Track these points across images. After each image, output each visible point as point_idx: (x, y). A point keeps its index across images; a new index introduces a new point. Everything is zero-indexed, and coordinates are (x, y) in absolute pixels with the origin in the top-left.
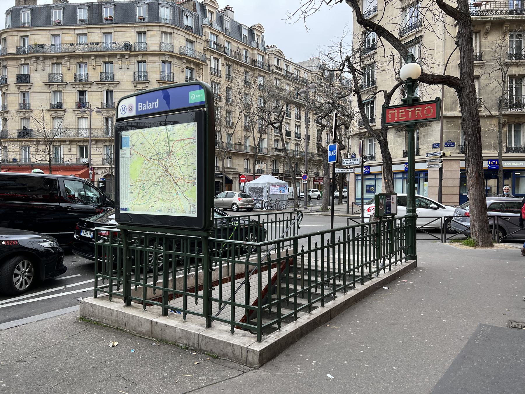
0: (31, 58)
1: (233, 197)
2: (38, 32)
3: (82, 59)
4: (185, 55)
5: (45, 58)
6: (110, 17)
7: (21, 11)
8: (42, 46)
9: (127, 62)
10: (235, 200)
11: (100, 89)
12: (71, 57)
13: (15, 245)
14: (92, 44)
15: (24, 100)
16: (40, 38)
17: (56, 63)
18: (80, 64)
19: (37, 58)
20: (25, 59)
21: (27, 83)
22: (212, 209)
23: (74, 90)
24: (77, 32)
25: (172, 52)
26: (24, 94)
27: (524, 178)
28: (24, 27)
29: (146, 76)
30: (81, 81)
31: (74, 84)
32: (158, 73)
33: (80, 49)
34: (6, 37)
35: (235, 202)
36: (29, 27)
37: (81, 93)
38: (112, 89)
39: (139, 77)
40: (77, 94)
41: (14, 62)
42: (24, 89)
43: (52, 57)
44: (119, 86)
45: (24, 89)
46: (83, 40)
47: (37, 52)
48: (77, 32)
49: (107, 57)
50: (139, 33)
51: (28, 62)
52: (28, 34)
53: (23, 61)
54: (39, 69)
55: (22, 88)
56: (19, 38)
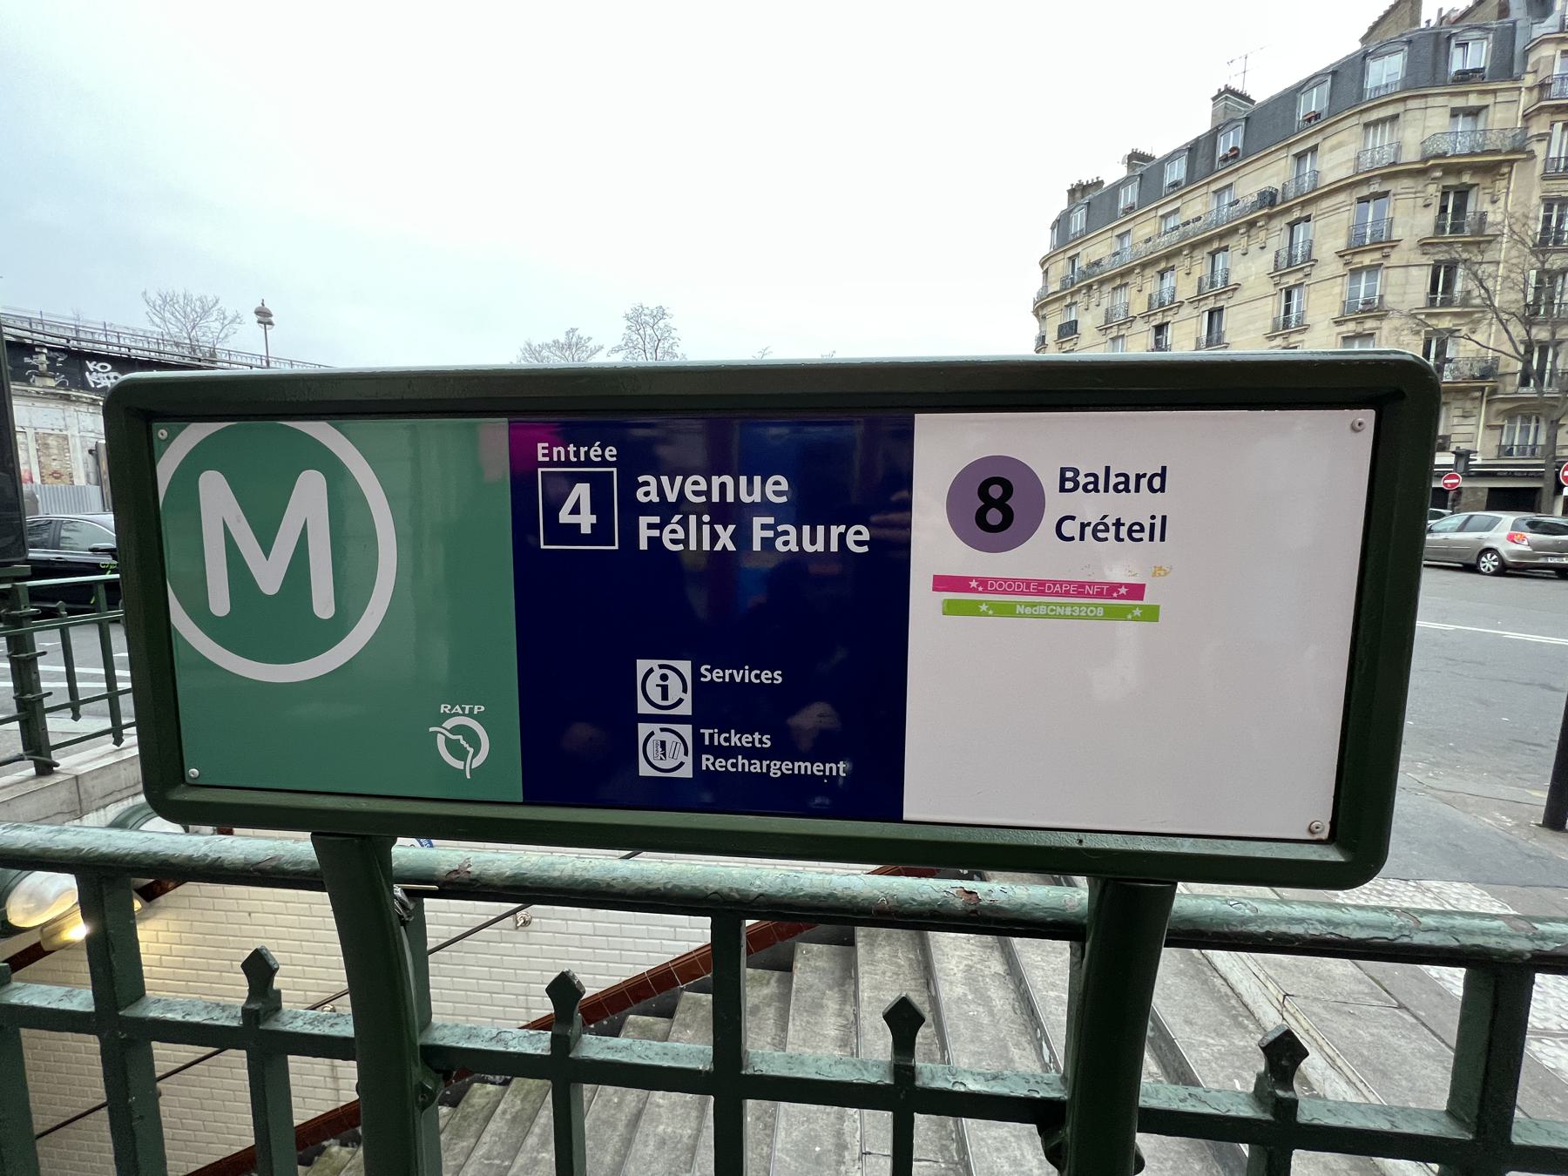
0: (1079, 290)
1: (1488, 528)
2: (1094, 241)
3: (1161, 262)
4: (1443, 155)
5: (1102, 282)
6: (1234, 149)
8: (1097, 263)
9: (1262, 234)
10: (1496, 540)
11: (1196, 313)
12: (1144, 266)
13: (133, 680)
14: (1188, 223)
15: (1288, 310)
16: (1099, 249)
17: (1120, 286)
18: (1162, 274)
19: (1090, 287)
23: (1146, 327)
24: (1161, 212)
25: (1394, 164)
29: (1308, 256)
30: (1161, 305)
31: (1146, 317)
32: (1344, 232)
33: (1164, 243)
35: (1494, 545)
37: (1215, 314)
38: (1219, 305)
39: (1291, 258)
40: (1153, 332)
41: (1056, 306)
43: (1112, 278)
44: (1237, 294)
46: (1172, 223)
47: (1090, 276)
48: (1161, 212)
49: (1214, 241)
50: (1300, 157)
51: (1077, 298)
52: (1079, 249)
53: (1068, 300)
54: (1092, 306)
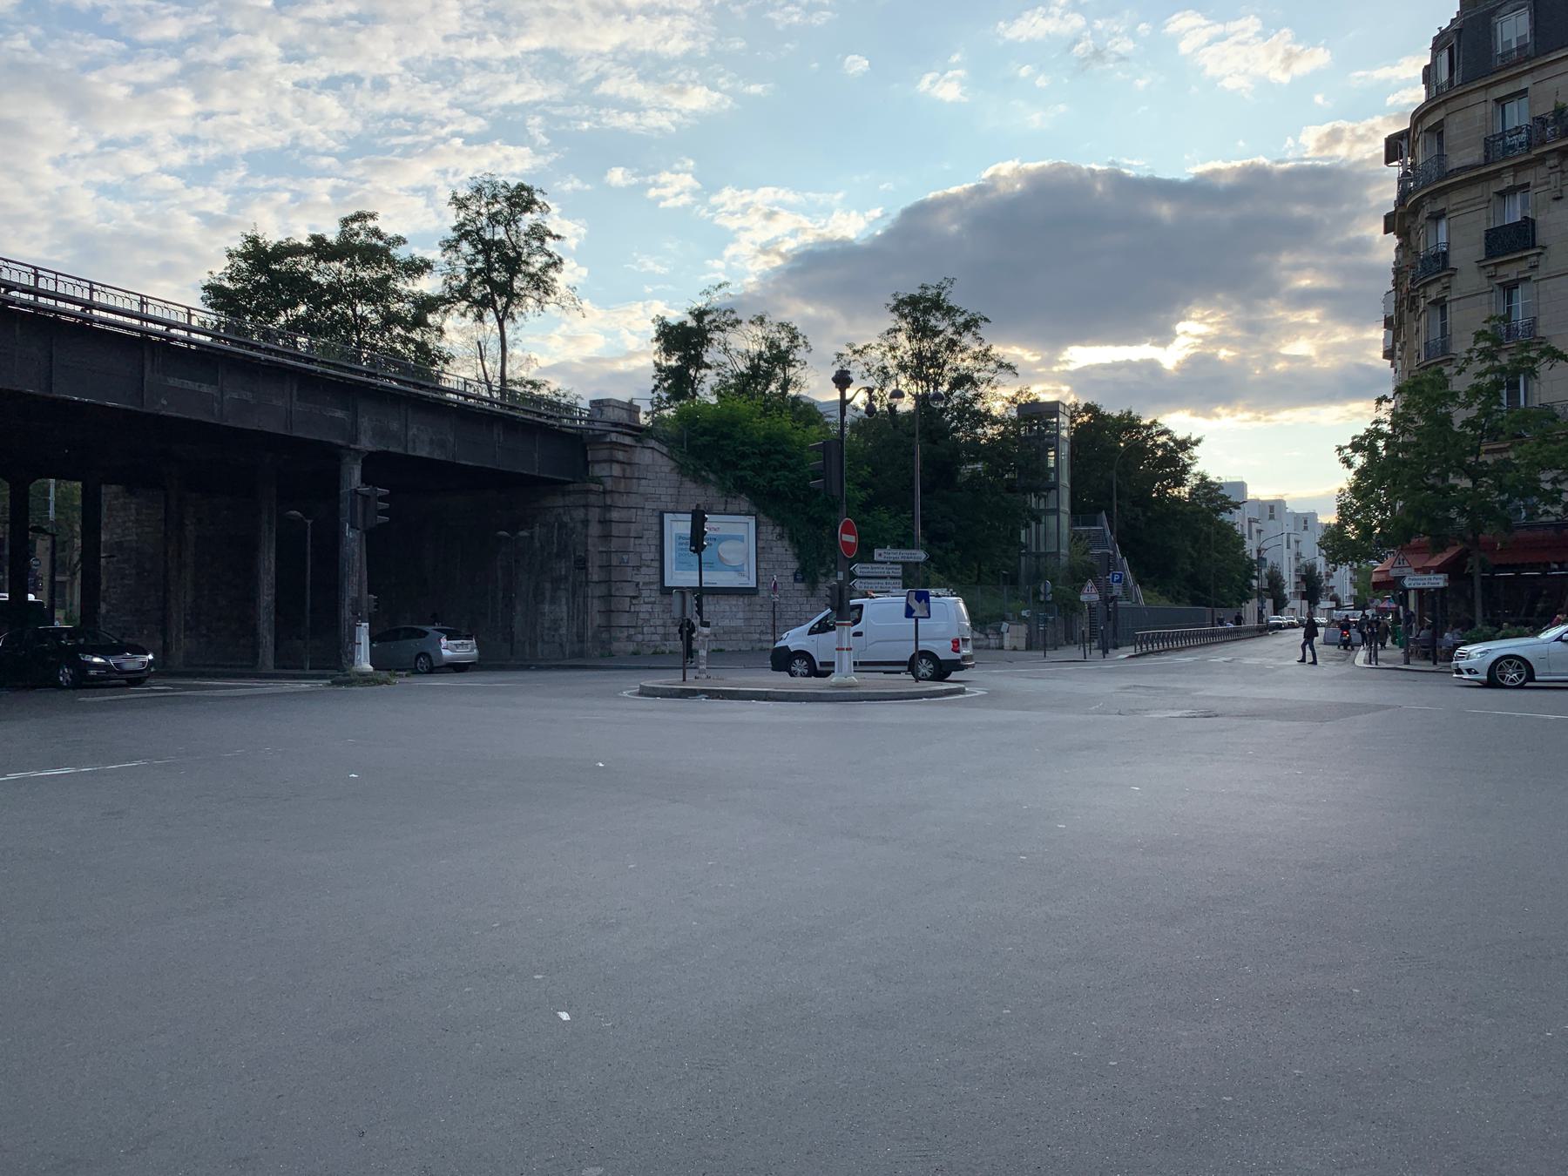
7: (1495, 20)
20: (1517, 168)
21: (1527, 249)
22: (1412, 608)
26: (1509, 288)
27: (1562, 363)
28: (1509, 67)
34: (1440, 123)
36: (1528, 59)
42: (1511, 272)
45: (1511, 272)
51: (1528, 176)
55: (1502, 271)
56: (1491, 106)
